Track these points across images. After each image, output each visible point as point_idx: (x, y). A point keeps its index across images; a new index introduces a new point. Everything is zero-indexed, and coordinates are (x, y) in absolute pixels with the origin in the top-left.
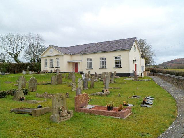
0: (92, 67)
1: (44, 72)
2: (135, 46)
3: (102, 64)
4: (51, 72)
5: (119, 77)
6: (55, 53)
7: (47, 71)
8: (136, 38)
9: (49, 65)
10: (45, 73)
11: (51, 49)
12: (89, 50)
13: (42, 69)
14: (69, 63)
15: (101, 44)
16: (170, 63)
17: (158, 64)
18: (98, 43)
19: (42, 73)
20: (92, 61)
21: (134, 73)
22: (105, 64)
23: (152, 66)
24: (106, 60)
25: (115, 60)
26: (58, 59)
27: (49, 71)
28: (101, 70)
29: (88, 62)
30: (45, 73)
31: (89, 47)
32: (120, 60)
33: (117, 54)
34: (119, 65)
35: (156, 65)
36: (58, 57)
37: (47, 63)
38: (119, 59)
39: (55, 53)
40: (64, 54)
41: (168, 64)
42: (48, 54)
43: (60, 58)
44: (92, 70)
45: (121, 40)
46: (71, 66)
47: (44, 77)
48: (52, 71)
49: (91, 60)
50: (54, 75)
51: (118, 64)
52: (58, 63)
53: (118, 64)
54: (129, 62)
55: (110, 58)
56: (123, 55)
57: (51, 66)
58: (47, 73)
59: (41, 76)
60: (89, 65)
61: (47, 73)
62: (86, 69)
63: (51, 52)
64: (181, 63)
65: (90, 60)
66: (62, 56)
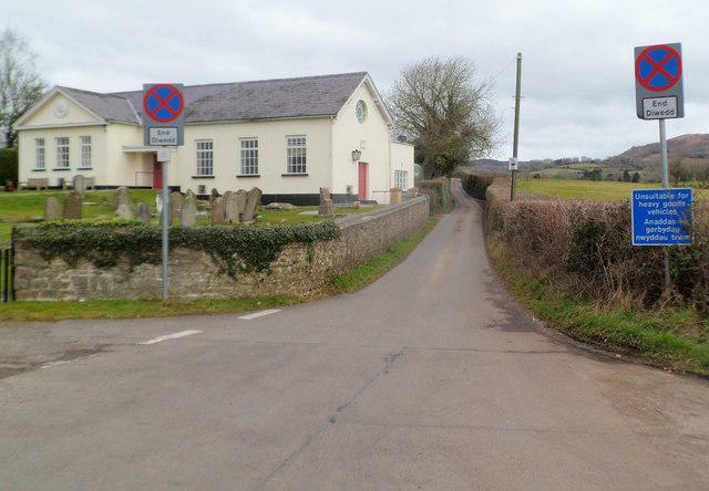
0: (304, 167)
1: (33, 185)
2: (20, 125)
3: (247, 160)
4: (60, 187)
5: (290, 206)
6: (77, 116)
7: (45, 181)
8: (365, 73)
9: (52, 159)
10: (34, 189)
11: (61, 102)
12: (204, 107)
13: (25, 174)
14: (131, 155)
15: (250, 87)
16: (654, 153)
17: (603, 157)
18: (241, 84)
19: (24, 189)
20: (256, 146)
21: (362, 198)
22: (256, 160)
23: (578, 166)
24: (260, 149)
25: (289, 150)
26: (87, 139)
27: (54, 183)
28: (237, 180)
29: (242, 152)
30: (34, 189)
31: (207, 99)
32: (305, 149)
33: (296, 129)
34: (299, 167)
35: (592, 162)
36: (86, 133)
37: (42, 151)
38: (209, 150)
39: (77, 116)
40: (111, 121)
41: (646, 155)
42: (48, 117)
43: (95, 134)
44: (212, 180)
45: (317, 78)
46: (139, 165)
47: (26, 203)
48: (62, 181)
49: (209, 145)
50: (53, 195)
51: (298, 166)
52: (87, 151)
53: (298, 166)
54: (330, 156)
55: (273, 142)
56: (311, 131)
57: (59, 164)
58: (43, 188)
59: (19, 199)
60: (247, 164)
61: (43, 188)
62: (238, 177)
63: (61, 111)
64: (701, 157)
65: (206, 147)
66: (102, 129)
